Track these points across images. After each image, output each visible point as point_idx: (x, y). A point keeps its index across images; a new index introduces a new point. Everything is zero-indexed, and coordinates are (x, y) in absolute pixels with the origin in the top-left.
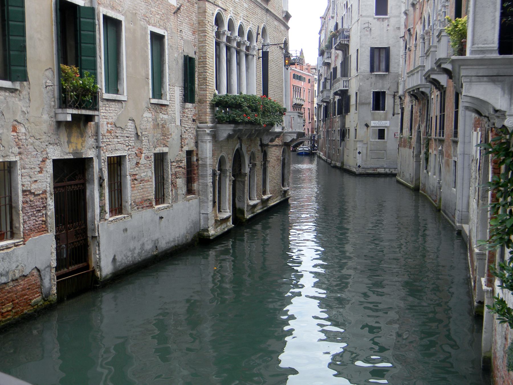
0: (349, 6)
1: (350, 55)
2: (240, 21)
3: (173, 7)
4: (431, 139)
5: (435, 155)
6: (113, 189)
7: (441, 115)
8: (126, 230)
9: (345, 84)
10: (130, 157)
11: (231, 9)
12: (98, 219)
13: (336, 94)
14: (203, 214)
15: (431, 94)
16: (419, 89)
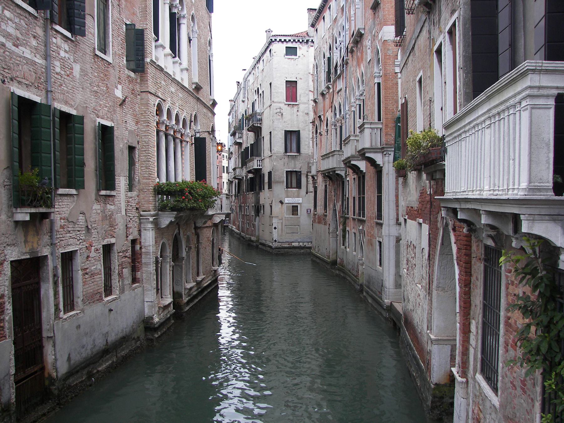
0: (260, 92)
1: (263, 137)
2: (176, 110)
3: (119, 100)
4: (348, 218)
5: (355, 233)
6: (65, 285)
7: (359, 198)
8: (78, 327)
9: (259, 163)
10: (81, 251)
11: (169, 99)
12: (53, 319)
13: (249, 172)
14: (147, 302)
15: (346, 176)
16: (335, 171)
